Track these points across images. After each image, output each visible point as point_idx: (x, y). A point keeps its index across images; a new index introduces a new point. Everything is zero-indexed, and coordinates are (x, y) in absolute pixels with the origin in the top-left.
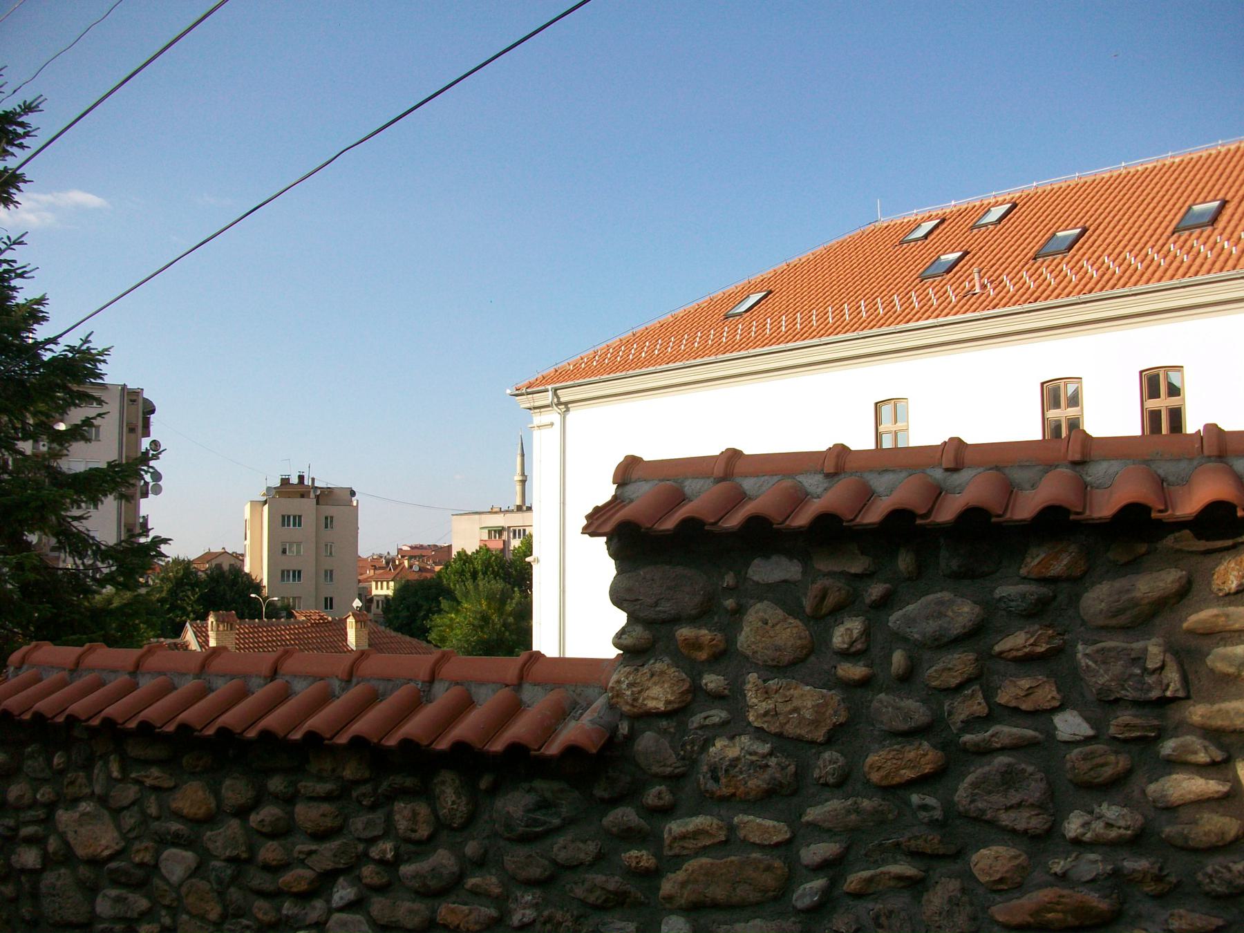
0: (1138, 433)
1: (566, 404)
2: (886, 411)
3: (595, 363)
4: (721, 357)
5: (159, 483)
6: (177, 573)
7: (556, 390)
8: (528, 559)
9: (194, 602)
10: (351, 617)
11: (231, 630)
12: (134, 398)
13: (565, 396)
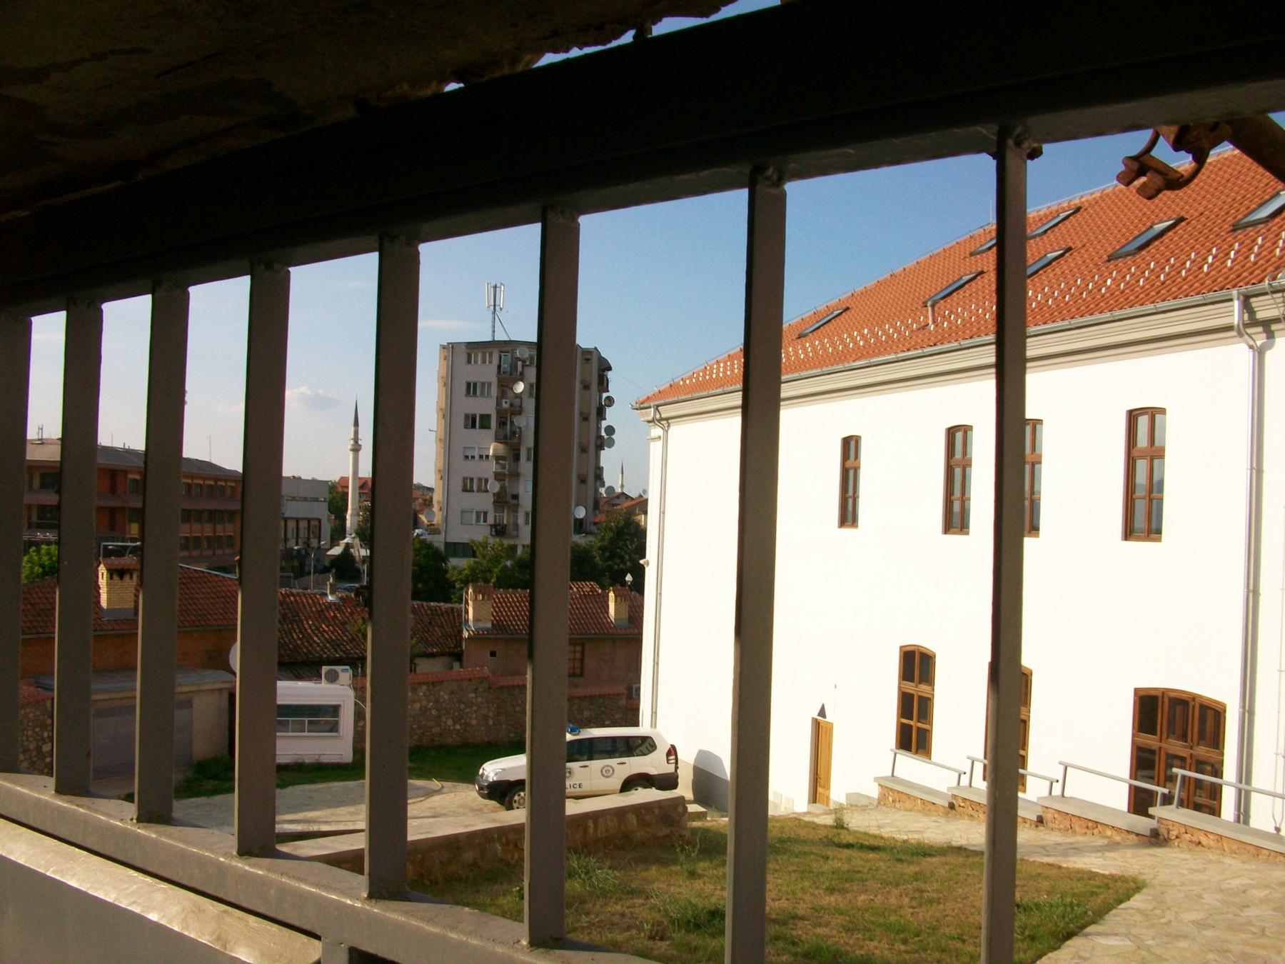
3: (1183, 273)
6: (618, 523)
7: (658, 406)
11: (488, 600)
12: (588, 357)
13: (666, 412)
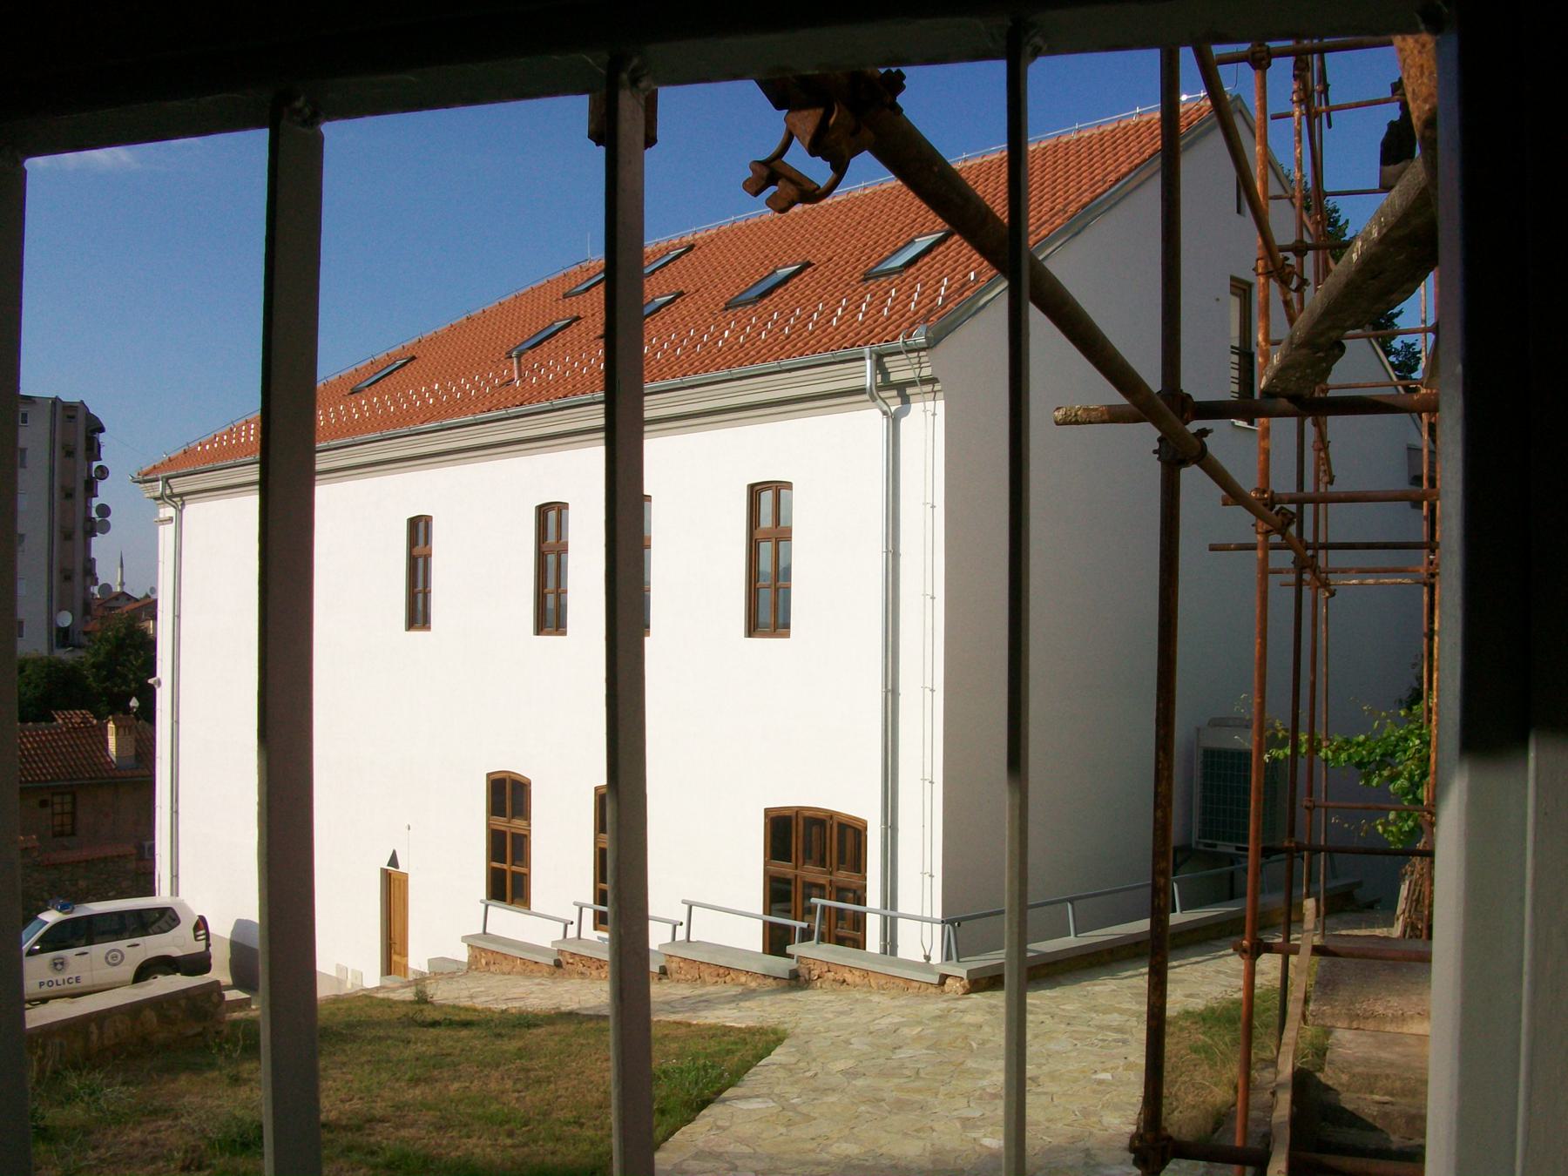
1: (181, 495)
2: (767, 498)
4: (787, 363)
7: (168, 478)
8: (151, 681)
10: (111, 722)
13: (179, 486)
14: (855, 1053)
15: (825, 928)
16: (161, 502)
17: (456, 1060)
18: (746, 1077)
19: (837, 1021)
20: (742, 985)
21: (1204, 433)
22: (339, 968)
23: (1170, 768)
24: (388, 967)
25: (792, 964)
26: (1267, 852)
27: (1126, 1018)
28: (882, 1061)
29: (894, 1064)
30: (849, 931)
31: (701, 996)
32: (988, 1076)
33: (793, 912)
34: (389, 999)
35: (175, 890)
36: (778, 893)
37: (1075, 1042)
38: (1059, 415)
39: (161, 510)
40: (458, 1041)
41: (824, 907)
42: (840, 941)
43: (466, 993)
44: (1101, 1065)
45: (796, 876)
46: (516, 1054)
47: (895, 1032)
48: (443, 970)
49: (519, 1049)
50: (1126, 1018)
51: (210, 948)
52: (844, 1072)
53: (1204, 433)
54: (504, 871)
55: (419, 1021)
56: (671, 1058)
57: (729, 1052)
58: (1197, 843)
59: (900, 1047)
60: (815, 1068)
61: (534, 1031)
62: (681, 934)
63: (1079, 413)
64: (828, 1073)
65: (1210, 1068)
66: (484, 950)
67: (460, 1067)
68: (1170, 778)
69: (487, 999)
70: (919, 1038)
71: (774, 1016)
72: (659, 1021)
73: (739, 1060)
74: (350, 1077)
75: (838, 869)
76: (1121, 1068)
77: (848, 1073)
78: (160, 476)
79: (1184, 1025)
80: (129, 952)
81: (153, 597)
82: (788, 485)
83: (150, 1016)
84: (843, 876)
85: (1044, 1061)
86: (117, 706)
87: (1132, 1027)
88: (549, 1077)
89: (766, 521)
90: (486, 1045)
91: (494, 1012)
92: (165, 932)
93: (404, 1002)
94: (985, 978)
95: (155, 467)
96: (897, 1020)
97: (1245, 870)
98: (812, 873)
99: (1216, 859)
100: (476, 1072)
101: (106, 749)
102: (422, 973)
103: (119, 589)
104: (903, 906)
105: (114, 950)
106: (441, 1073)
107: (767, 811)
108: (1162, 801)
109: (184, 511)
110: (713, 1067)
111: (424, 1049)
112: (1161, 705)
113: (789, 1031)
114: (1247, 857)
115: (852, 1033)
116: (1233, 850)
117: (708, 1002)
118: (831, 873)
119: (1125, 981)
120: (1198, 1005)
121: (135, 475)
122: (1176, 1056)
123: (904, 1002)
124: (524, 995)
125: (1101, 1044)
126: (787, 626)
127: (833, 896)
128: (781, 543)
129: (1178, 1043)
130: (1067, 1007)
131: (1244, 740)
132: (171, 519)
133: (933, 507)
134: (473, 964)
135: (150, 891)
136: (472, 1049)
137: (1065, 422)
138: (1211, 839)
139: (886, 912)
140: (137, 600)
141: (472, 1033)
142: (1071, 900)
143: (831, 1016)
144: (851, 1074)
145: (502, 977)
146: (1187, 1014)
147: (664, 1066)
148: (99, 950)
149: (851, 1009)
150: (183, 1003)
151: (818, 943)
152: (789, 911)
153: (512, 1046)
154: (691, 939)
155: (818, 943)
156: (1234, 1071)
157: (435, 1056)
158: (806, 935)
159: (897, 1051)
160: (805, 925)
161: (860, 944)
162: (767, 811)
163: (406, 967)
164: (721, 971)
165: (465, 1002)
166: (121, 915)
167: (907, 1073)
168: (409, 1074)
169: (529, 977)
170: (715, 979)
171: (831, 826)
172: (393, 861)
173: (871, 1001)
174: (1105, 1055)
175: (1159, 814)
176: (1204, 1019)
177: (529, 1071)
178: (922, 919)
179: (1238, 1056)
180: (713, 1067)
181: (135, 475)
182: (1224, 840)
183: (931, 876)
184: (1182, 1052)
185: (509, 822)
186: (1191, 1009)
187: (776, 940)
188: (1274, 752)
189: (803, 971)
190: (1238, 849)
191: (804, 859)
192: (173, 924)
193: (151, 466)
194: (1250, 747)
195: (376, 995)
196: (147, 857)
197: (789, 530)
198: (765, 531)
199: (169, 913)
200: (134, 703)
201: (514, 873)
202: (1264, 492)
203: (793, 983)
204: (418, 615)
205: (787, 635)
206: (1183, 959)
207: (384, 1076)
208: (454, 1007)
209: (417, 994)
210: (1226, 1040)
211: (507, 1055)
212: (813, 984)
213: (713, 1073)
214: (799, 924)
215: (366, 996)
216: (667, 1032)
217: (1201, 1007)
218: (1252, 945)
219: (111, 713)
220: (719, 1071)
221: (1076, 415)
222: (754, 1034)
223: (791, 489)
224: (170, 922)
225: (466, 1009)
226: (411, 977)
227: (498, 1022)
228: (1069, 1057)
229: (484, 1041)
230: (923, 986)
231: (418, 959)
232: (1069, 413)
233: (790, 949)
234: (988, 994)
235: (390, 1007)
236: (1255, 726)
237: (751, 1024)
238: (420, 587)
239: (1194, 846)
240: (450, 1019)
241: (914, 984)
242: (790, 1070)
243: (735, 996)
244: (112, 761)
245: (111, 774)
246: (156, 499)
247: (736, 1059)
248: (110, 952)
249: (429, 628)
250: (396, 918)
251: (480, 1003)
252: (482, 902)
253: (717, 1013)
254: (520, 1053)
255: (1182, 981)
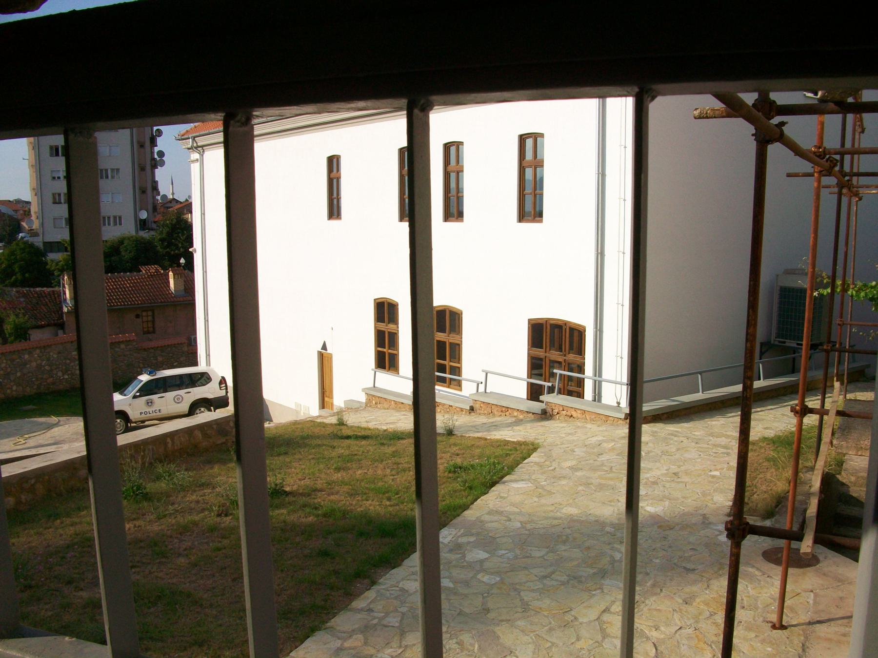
0: (531, 159)
1: (202, 147)
2: (529, 143)
5: (163, 158)
7: (195, 137)
8: (191, 250)
9: (184, 241)
13: (201, 141)
14: (577, 457)
15: (561, 385)
16: (191, 150)
17: (360, 458)
18: (516, 469)
19: (567, 438)
20: (515, 417)
21: (783, 124)
22: (297, 404)
23: (755, 320)
24: (323, 405)
25: (543, 406)
26: (813, 347)
27: (729, 440)
28: (591, 461)
29: (598, 463)
30: (575, 389)
31: (492, 423)
32: (650, 472)
33: (544, 376)
34: (323, 423)
35: (208, 363)
36: (536, 366)
37: (700, 453)
38: (697, 113)
39: (192, 155)
40: (361, 447)
41: (561, 375)
42: (570, 393)
43: (364, 420)
44: (714, 467)
45: (546, 357)
46: (392, 455)
47: (599, 445)
48: (352, 407)
49: (394, 452)
50: (729, 440)
51: (228, 394)
52: (571, 468)
53: (783, 124)
54: (384, 353)
55: (340, 436)
56: (476, 458)
57: (507, 455)
58: (775, 341)
59: (602, 454)
60: (555, 465)
61: (401, 441)
62: (482, 388)
63: (708, 112)
64: (562, 468)
65: (776, 470)
66: (374, 396)
67: (362, 462)
68: (755, 325)
69: (375, 423)
70: (613, 449)
71: (532, 435)
72: (470, 437)
73: (513, 459)
74: (303, 467)
75: (569, 353)
76: (725, 469)
77: (573, 468)
78: (190, 136)
79: (763, 445)
80: (186, 396)
81: (190, 201)
82: (542, 135)
83: (198, 434)
84: (571, 357)
85: (682, 464)
86: (173, 262)
87: (732, 446)
88: (410, 468)
89: (529, 156)
90: (376, 450)
91: (380, 431)
92: (204, 385)
93: (331, 424)
94: (650, 416)
95: (187, 131)
96: (600, 438)
97: (801, 356)
98: (555, 355)
99: (785, 350)
100: (370, 465)
101: (169, 286)
102: (341, 408)
103: (171, 197)
104: (605, 375)
105: (178, 395)
106: (352, 465)
107: (530, 320)
108: (751, 322)
109: (204, 155)
110: (499, 463)
111: (343, 451)
112: (752, 283)
113: (541, 444)
114: (802, 349)
115: (575, 446)
116: (796, 346)
117: (496, 427)
118: (565, 356)
119: (731, 419)
120: (770, 434)
121: (177, 136)
122: (757, 463)
123: (605, 428)
124: (396, 421)
125: (714, 455)
126: (540, 215)
127: (566, 368)
128: (538, 168)
129: (758, 455)
130: (696, 433)
131: (803, 283)
132: (197, 160)
133: (625, 147)
134: (368, 404)
135: (195, 363)
136: (368, 451)
137: (700, 117)
138: (782, 338)
139: (595, 378)
140: (181, 203)
141: (368, 443)
142: (700, 373)
143: (564, 436)
144: (574, 469)
145: (383, 411)
146: (765, 439)
147: (472, 463)
148: (170, 395)
149: (575, 432)
150: (215, 426)
151: (557, 395)
152: (541, 375)
153: (389, 450)
154: (487, 391)
155: (557, 395)
156: (789, 473)
157: (348, 455)
158: (551, 390)
159: (600, 456)
160: (550, 384)
161: (580, 395)
162: (530, 320)
163: (332, 404)
164: (504, 409)
165: (364, 425)
166: (181, 377)
167: (606, 468)
168: (335, 465)
169: (398, 411)
170: (500, 413)
171: (566, 329)
172: (324, 347)
173: (586, 427)
174: (717, 461)
175: (749, 345)
176: (774, 442)
177: (399, 464)
178: (616, 383)
179: (792, 462)
180: (499, 463)
181: (177, 136)
182: (790, 339)
183: (622, 358)
184: (760, 461)
185: (387, 326)
186: (766, 436)
187: (534, 393)
188: (821, 291)
189: (549, 410)
190: (798, 344)
191: (550, 347)
192: (208, 381)
193: (185, 131)
194: (805, 286)
195: (316, 420)
196: (193, 344)
197: (543, 161)
198: (529, 162)
199: (206, 375)
200: (182, 261)
201: (389, 354)
202: (820, 148)
203: (543, 416)
204: (334, 211)
205: (541, 221)
206: (763, 407)
207: (322, 466)
208: (358, 427)
209: (338, 420)
210: (785, 455)
211: (387, 455)
212: (554, 417)
213: (499, 467)
214: (547, 384)
215: (312, 421)
216: (473, 443)
217: (772, 435)
218: (801, 409)
219: (171, 266)
220: (502, 466)
221: (706, 113)
222: (521, 445)
223: (543, 137)
224: (207, 380)
225: (365, 429)
226: (335, 411)
227: (381, 437)
228: (696, 462)
229: (374, 447)
230: (616, 419)
231: (339, 400)
232: (702, 112)
233: (541, 398)
234: (652, 424)
235: (324, 427)
236: (809, 275)
237: (520, 439)
238: (335, 195)
239: (772, 342)
240: (356, 435)
241: (611, 418)
242: (541, 466)
243: (511, 423)
244: (172, 293)
245: (172, 300)
246: (189, 149)
247: (511, 459)
248: (176, 396)
249: (340, 218)
250: (326, 370)
251: (371, 425)
252: (372, 370)
253: (501, 433)
254: (395, 454)
255: (763, 420)
